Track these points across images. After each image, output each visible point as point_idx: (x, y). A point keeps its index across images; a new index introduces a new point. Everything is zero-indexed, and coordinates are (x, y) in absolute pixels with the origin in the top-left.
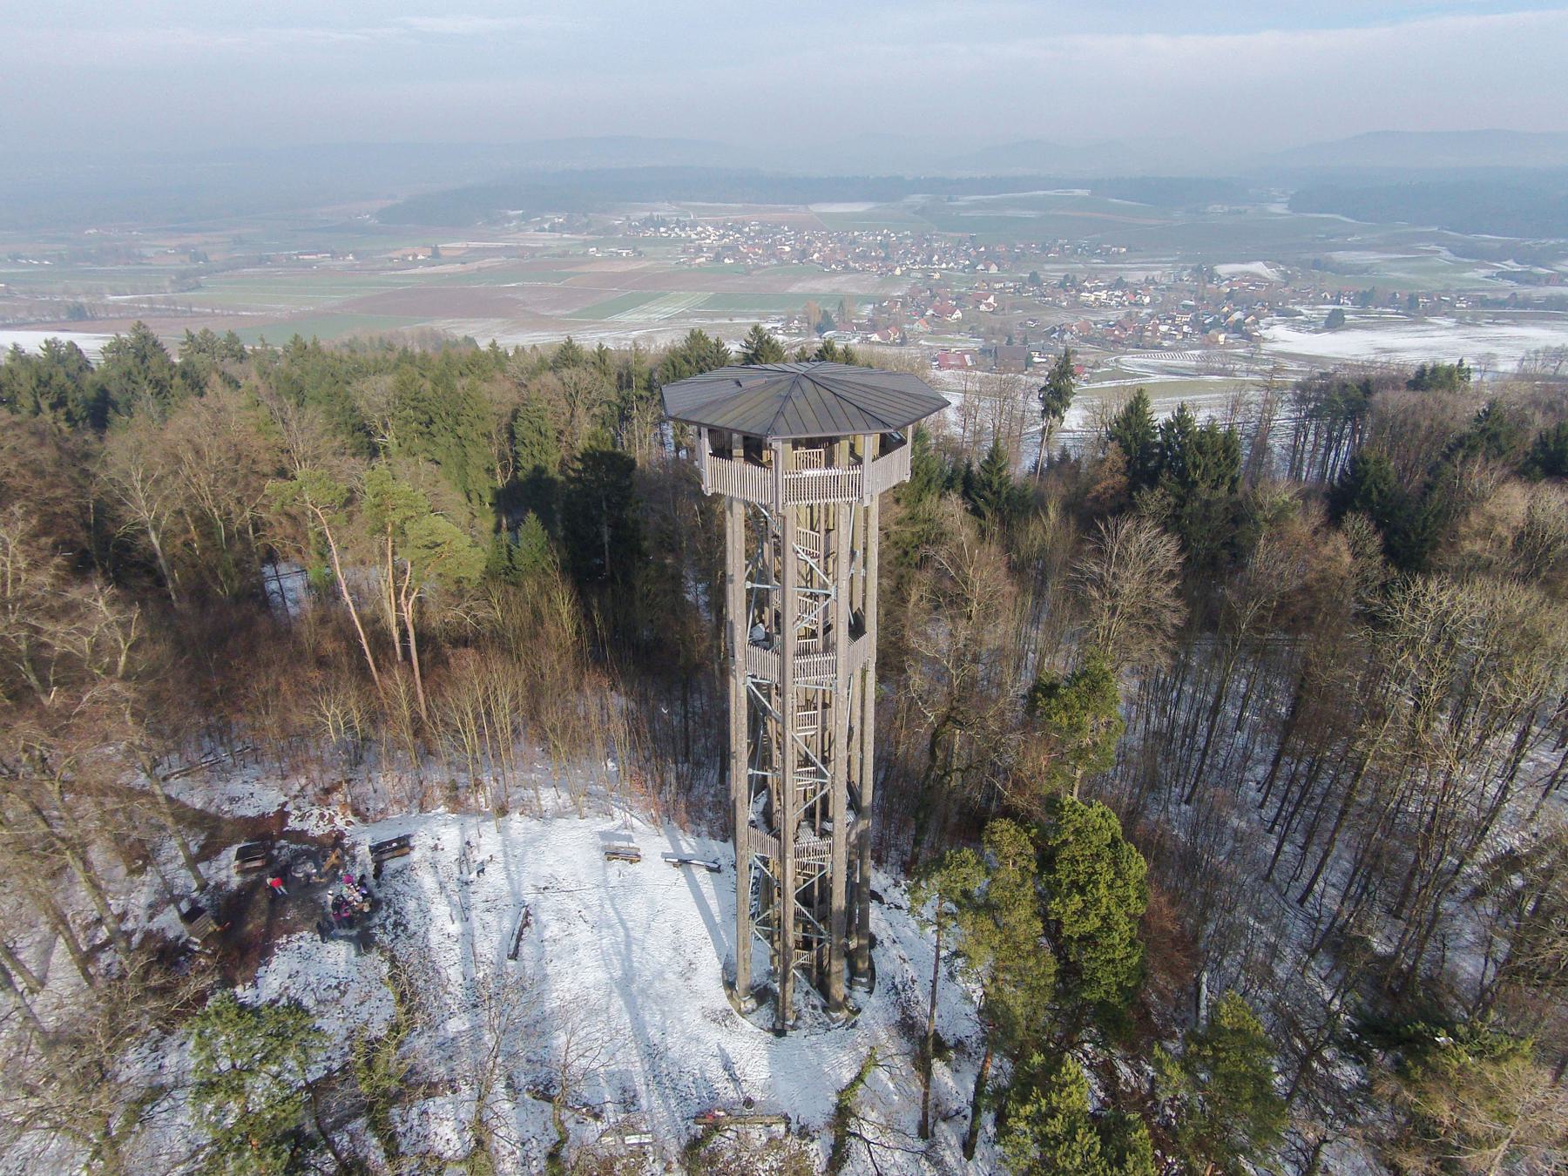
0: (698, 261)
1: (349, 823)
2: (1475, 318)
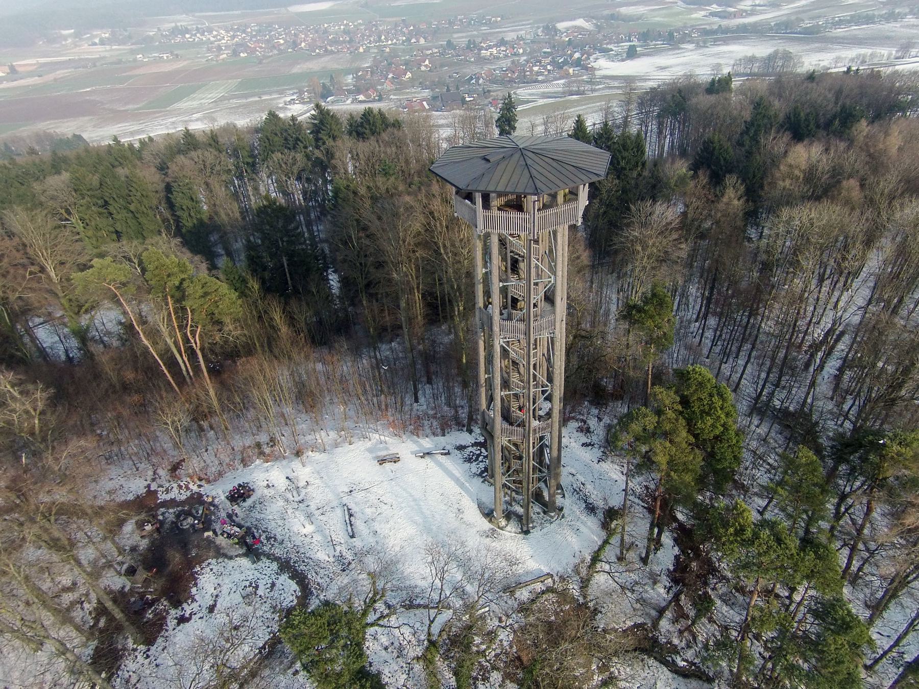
0: (221, 57)
1: (200, 486)
2: (705, 42)
